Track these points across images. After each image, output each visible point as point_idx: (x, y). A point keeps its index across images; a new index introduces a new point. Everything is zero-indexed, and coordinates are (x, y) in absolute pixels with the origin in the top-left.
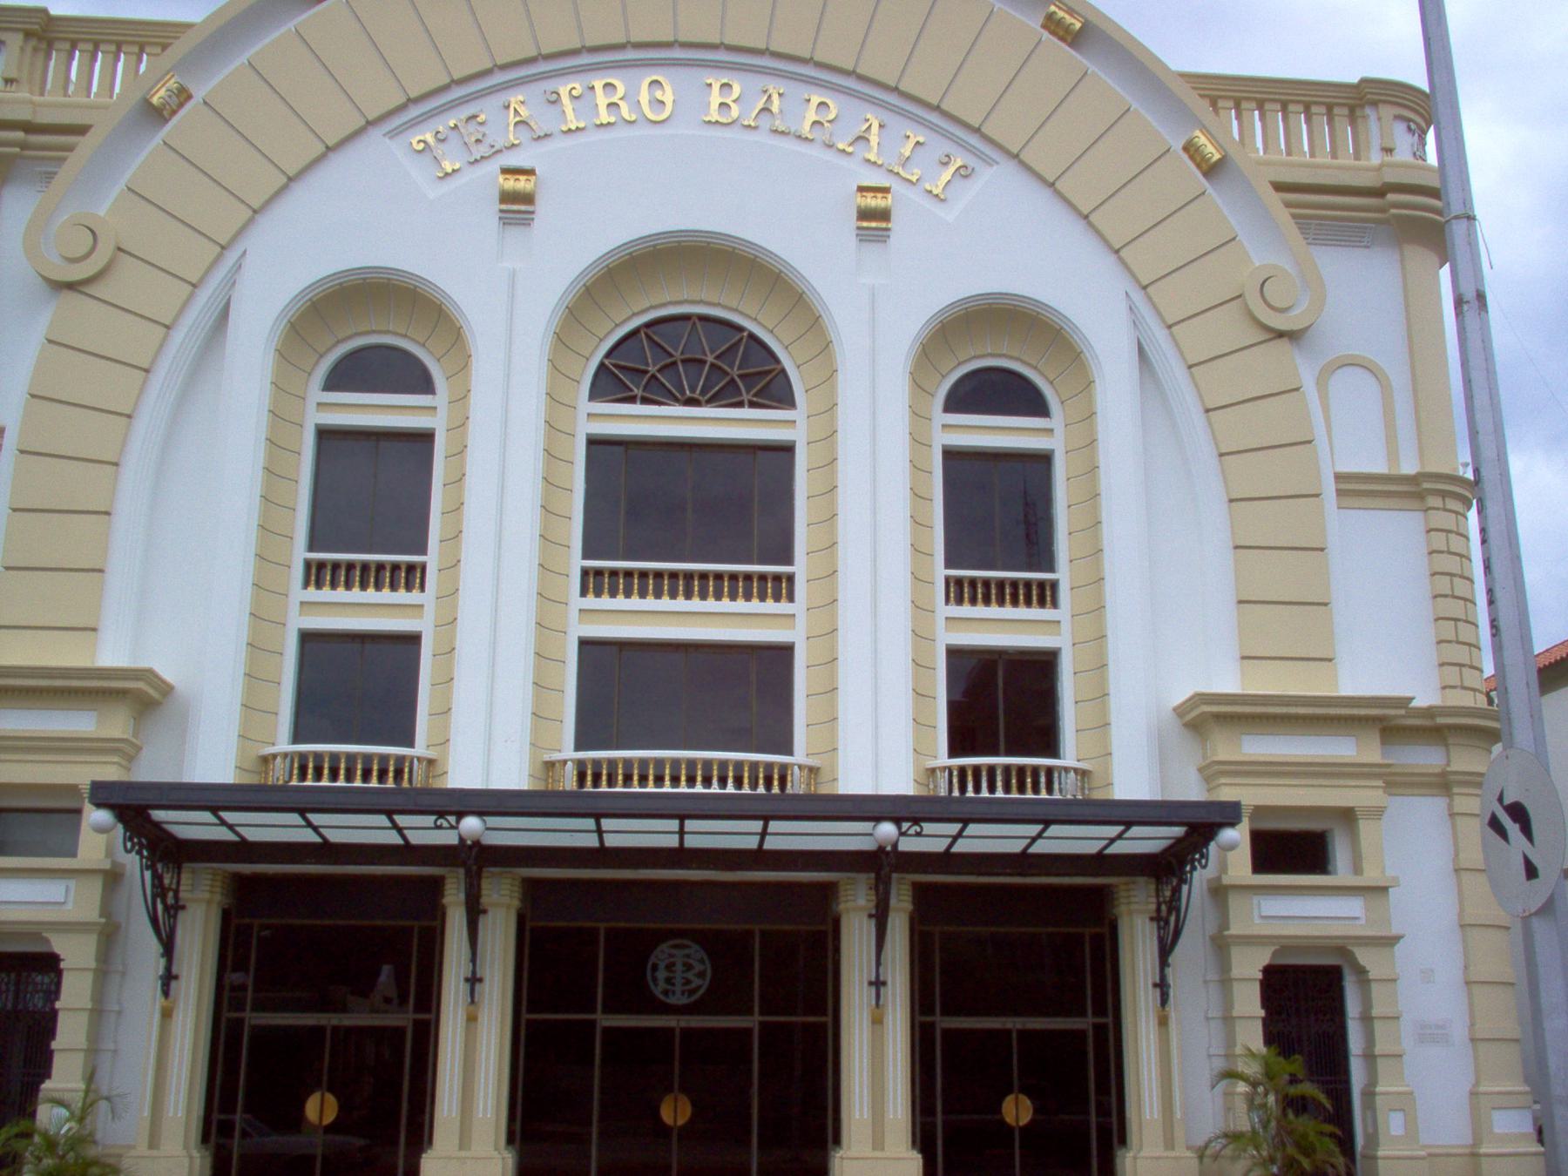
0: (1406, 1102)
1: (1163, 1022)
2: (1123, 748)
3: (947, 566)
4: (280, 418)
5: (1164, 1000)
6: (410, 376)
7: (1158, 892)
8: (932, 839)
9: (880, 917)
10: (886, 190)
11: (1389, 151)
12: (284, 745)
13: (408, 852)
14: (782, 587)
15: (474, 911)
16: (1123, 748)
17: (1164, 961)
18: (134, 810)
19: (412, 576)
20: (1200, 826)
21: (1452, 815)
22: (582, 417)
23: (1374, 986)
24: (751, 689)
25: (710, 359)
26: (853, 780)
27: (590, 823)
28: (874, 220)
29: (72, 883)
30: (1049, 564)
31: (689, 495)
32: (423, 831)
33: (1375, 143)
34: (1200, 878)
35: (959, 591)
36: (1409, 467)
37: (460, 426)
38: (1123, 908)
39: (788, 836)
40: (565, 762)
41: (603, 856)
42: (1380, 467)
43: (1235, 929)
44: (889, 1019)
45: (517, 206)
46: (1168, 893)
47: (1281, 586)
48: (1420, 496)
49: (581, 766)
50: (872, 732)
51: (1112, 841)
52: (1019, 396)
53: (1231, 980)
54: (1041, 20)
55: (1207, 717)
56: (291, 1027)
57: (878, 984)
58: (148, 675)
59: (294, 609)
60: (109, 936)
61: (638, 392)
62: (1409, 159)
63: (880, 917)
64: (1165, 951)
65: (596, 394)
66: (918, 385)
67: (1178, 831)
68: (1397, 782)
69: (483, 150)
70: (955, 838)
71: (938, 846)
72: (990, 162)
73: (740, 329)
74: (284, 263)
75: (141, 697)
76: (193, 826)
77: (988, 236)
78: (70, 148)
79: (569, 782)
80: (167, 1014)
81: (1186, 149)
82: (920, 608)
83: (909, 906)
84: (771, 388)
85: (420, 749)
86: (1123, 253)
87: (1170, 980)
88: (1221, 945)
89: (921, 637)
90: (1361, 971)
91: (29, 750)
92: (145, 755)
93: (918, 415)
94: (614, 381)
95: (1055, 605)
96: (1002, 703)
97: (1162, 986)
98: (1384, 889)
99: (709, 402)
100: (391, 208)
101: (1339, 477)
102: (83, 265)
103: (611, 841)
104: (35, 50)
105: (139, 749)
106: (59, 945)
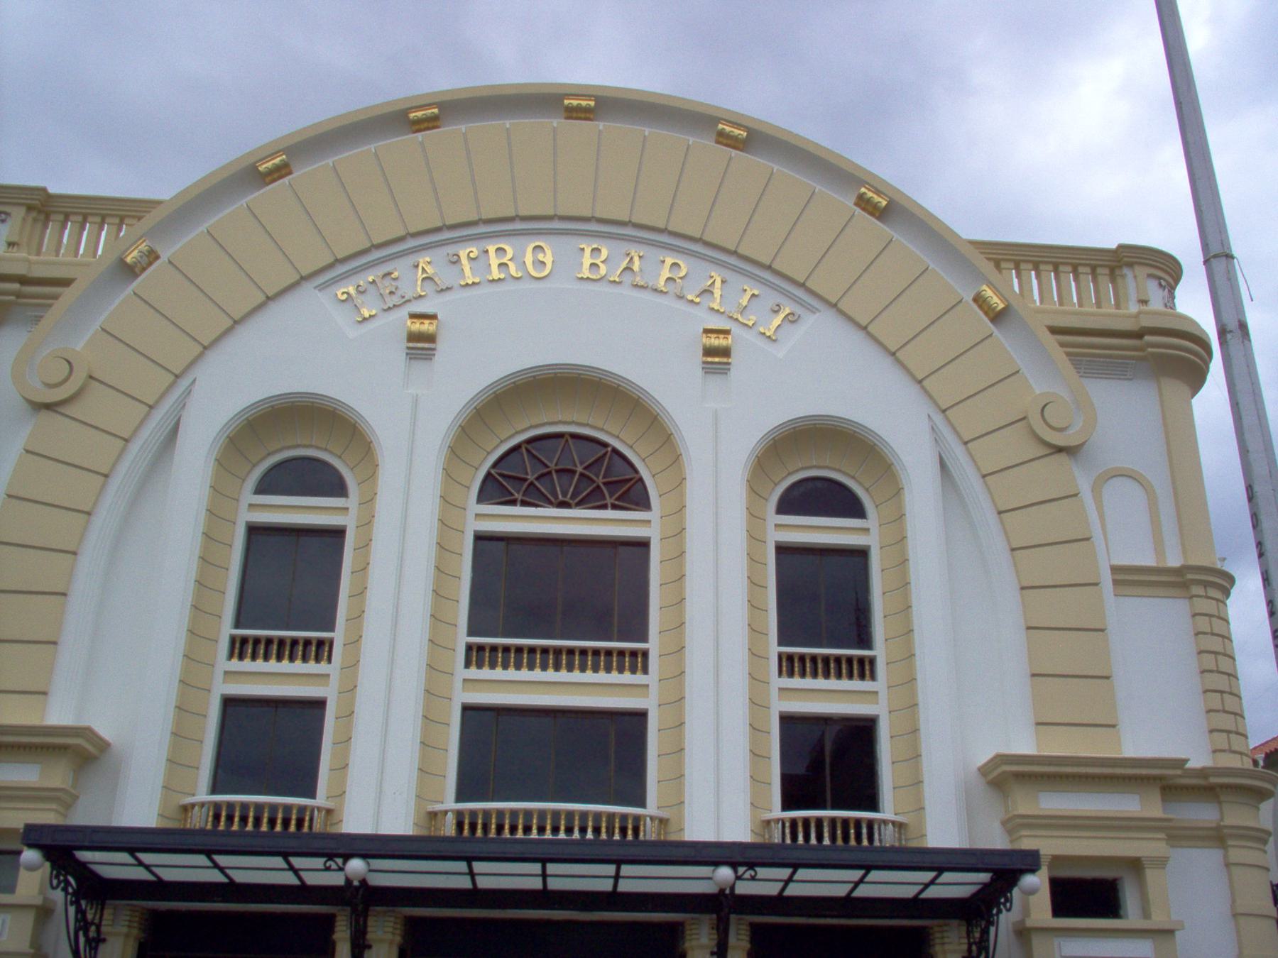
2: (935, 798)
3: (780, 644)
4: (216, 516)
6: (327, 482)
7: (969, 933)
8: (766, 882)
10: (726, 332)
11: (1144, 302)
13: (303, 892)
14: (321, 650)
16: (935, 798)
18: (61, 849)
19: (321, 650)
20: (1005, 872)
21: (1228, 865)
22: (771, 527)
24: (611, 749)
28: (717, 357)
31: (559, 583)
32: (316, 872)
33: (1133, 297)
34: (1006, 920)
35: (789, 665)
39: (639, 879)
40: (446, 812)
41: (475, 896)
42: (1149, 561)
45: (421, 344)
46: (977, 935)
47: (1068, 665)
48: (1185, 585)
51: (927, 886)
55: (1008, 776)
58: (86, 732)
61: (518, 496)
65: (483, 497)
66: (448, 475)
67: (984, 877)
68: (1179, 835)
70: (787, 882)
72: (813, 310)
74: (231, 385)
75: (81, 752)
76: (113, 866)
77: (810, 369)
78: (55, 297)
79: (449, 829)
81: (975, 300)
82: (756, 679)
84: (630, 493)
91: (1129, 828)
93: (754, 516)
94: (497, 487)
95: (873, 678)
96: (831, 764)
99: (580, 504)
100: (320, 346)
104: (35, 220)
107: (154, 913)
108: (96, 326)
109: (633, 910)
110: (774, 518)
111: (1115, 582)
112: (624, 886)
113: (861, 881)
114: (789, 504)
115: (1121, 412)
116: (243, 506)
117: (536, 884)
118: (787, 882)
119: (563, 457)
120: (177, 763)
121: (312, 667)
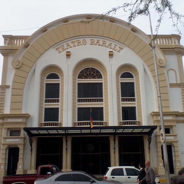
0: (179, 161)
1: (149, 152)
2: (144, 119)
4: (42, 83)
5: (149, 150)
6: (56, 77)
7: (149, 137)
8: (120, 131)
9: (115, 140)
10: (112, 52)
11: (175, 43)
12: (77, 122)
13: (59, 134)
15: (67, 141)
16: (144, 119)
17: (149, 145)
18: (28, 130)
19: (58, 101)
20: (153, 128)
22: (120, 80)
23: (175, 148)
24: (98, 113)
25: (92, 73)
26: (110, 124)
27: (80, 130)
28: (111, 55)
29: (20, 139)
30: (134, 96)
31: (90, 90)
32: (61, 132)
33: (173, 42)
34: (153, 135)
36: (179, 82)
37: (63, 83)
38: (144, 139)
39: (103, 131)
40: (76, 123)
41: (81, 134)
42: (175, 82)
43: (158, 141)
44: (33, 154)
45: (68, 55)
47: (163, 97)
48: (180, 86)
49: (78, 123)
50: (112, 118)
52: (129, 75)
53: (175, 147)
54: (131, 29)
55: (156, 114)
56: (172, 150)
57: (115, 148)
58: (28, 114)
59: (44, 105)
60: (24, 145)
61: (96, 77)
62: (178, 44)
63: (115, 140)
64: (149, 143)
65: (78, 78)
66: (74, 75)
67: (150, 129)
68: (178, 122)
69: (64, 49)
70: (123, 131)
71: (121, 132)
72: (125, 47)
73: (95, 69)
74: (41, 65)
75: (27, 117)
76: (35, 132)
77: (127, 56)
78: (16, 52)
80: (31, 154)
81: (149, 44)
82: (118, 102)
83: (118, 139)
84: (100, 77)
85: (104, 121)
86: (38, 57)
87: (150, 147)
88: (156, 143)
89: (118, 106)
90: (174, 145)
91: (10, 124)
92: (28, 124)
93: (117, 79)
94: (80, 77)
95: (135, 101)
96: (129, 114)
97: (149, 148)
98: (176, 135)
100: (52, 57)
101: (170, 84)
102: (161, 65)
103: (82, 132)
104: (11, 40)
105: (27, 123)
106: (19, 146)
107: (39, 138)
108: (22, 56)
109: (82, 135)
110: (120, 79)
111: (170, 86)
112: (101, 132)
113: (133, 130)
114: (122, 76)
115: (172, 59)
116: (45, 81)
117: (80, 132)
118: (123, 131)
119: (89, 71)
120: (40, 117)
121: (56, 103)
